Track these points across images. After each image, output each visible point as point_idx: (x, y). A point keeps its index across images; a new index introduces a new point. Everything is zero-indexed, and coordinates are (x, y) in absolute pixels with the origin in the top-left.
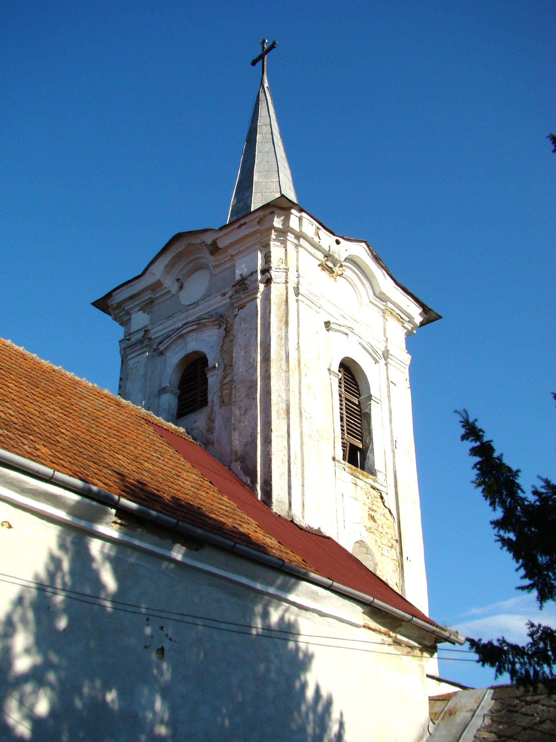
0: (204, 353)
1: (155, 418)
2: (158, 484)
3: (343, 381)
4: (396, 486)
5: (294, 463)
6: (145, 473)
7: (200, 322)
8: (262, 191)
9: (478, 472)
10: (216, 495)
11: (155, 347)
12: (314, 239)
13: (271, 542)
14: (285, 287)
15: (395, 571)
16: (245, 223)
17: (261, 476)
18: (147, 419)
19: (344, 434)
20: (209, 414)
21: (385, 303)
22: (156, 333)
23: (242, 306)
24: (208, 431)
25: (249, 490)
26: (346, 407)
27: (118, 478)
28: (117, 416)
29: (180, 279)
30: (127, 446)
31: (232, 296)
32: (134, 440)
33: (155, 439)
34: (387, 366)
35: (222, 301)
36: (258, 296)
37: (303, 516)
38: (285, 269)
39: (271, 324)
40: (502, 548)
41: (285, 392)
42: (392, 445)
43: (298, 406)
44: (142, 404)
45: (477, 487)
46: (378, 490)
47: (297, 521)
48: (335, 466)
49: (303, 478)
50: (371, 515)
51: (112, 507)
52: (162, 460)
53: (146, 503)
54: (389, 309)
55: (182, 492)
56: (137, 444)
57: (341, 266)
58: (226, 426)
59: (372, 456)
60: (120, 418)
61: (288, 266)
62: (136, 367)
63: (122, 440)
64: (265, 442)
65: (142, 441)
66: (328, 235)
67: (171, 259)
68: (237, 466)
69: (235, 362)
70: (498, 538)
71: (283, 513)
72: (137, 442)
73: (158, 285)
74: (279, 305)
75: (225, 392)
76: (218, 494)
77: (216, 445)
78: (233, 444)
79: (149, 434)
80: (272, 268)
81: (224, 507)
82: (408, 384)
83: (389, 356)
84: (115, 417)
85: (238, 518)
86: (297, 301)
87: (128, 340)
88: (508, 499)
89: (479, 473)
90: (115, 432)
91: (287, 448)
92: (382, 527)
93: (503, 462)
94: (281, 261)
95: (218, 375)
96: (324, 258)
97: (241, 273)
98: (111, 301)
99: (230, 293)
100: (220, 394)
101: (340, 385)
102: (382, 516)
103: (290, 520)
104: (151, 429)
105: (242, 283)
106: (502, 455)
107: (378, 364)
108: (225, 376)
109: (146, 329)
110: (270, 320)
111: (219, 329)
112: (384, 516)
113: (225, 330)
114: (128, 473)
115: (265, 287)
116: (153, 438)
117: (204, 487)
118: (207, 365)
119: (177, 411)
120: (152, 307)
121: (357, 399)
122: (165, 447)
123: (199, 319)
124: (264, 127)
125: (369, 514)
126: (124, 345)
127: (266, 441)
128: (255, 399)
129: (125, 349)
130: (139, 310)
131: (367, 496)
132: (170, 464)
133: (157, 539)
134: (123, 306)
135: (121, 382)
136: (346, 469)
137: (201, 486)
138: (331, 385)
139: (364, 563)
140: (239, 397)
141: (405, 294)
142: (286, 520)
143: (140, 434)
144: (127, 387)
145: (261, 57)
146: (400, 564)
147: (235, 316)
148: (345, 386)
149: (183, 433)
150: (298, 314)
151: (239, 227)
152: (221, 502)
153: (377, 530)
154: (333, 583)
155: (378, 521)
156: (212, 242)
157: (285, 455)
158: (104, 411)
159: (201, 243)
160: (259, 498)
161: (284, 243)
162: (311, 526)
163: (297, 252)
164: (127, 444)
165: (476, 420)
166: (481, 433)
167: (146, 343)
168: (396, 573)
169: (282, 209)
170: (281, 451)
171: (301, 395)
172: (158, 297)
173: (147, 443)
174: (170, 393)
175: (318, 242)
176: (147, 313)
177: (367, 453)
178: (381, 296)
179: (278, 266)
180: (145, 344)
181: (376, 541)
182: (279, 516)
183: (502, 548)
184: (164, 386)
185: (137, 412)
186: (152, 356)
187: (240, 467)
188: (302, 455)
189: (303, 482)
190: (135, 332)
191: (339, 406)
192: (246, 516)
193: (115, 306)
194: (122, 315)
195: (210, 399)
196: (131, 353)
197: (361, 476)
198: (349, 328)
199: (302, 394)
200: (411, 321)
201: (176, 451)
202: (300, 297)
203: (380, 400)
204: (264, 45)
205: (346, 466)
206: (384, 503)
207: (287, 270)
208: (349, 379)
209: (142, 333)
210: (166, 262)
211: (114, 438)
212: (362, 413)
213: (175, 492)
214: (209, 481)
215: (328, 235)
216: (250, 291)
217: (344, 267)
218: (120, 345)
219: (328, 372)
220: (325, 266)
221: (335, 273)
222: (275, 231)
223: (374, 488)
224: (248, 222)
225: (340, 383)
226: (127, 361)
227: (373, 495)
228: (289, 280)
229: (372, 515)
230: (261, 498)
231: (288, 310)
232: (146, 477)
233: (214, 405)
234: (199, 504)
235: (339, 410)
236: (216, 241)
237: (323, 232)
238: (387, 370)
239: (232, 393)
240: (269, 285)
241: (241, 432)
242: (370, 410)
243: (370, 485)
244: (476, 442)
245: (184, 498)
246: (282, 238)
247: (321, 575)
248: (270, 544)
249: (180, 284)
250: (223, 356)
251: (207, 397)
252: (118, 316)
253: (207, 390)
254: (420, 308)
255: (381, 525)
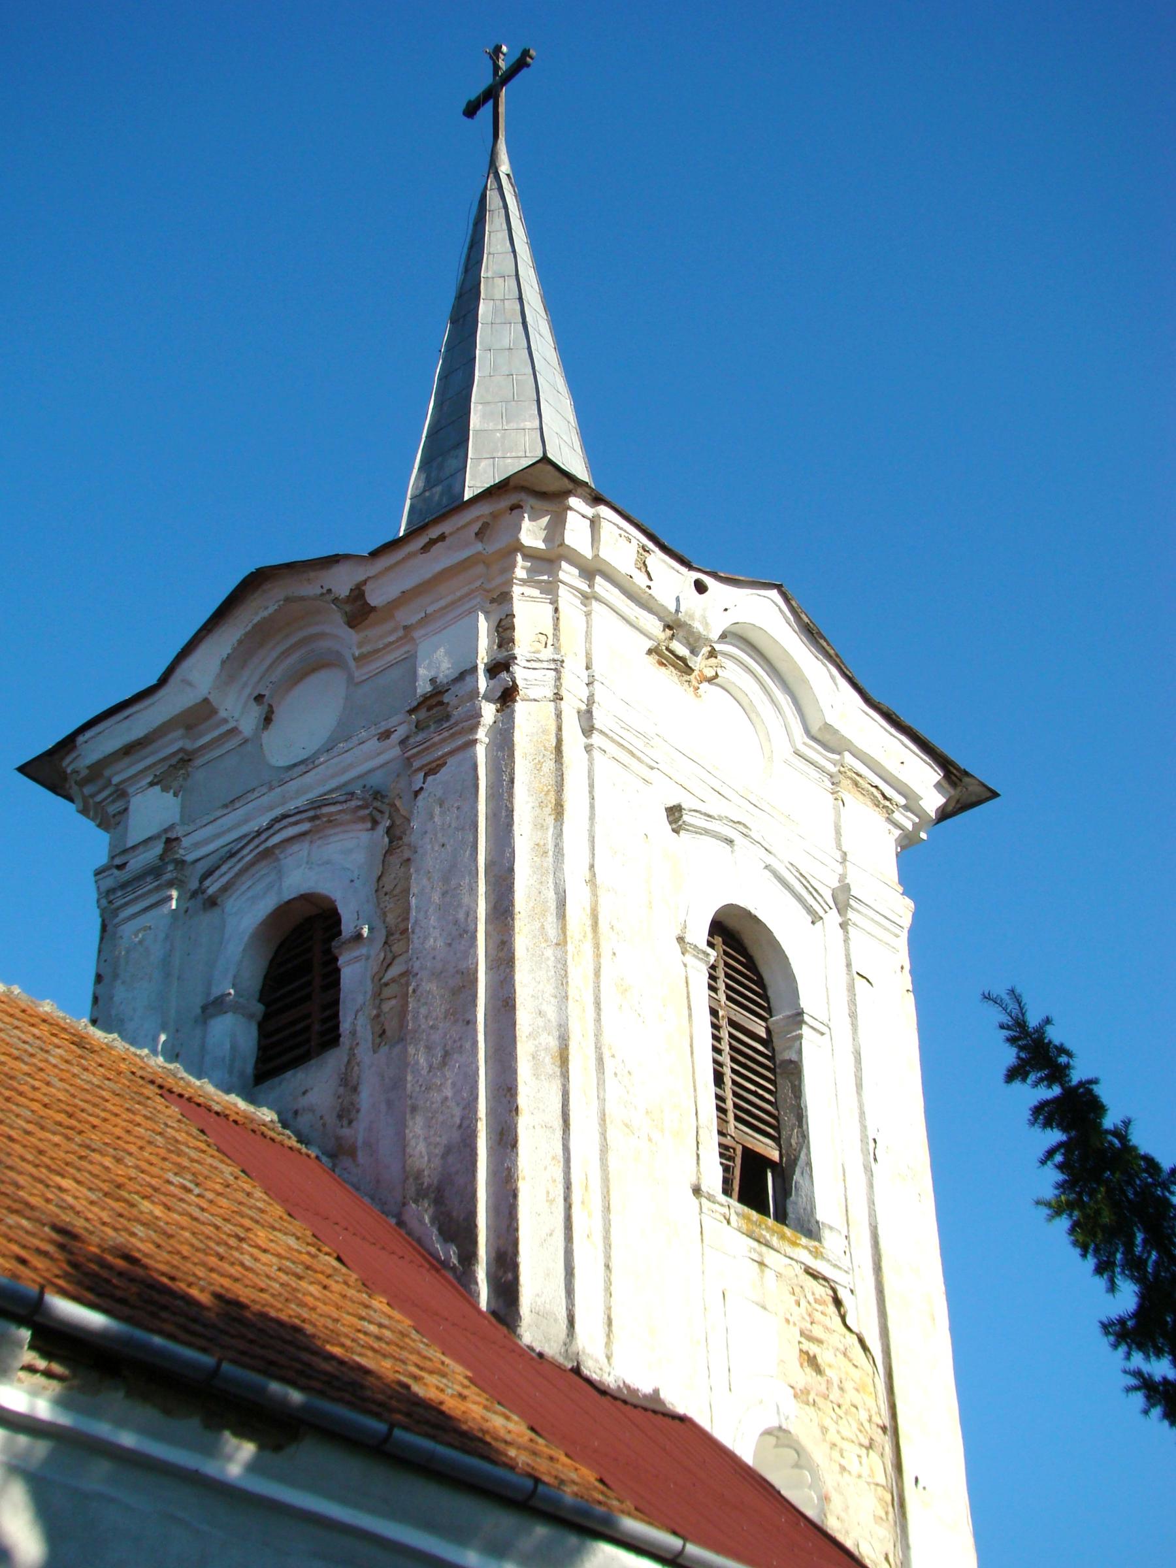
0: (331, 899)
1: (188, 1084)
2: (176, 1260)
3: (720, 974)
4: (878, 1269)
5: (583, 1203)
6: (139, 1230)
7: (318, 812)
8: (495, 455)
9: (1059, 1177)
10: (351, 1292)
11: (194, 885)
12: (635, 580)
13: (506, 1428)
14: (553, 711)
15: (881, 1518)
16: (442, 538)
17: (487, 1241)
18: (165, 1084)
19: (727, 1122)
20: (343, 1070)
21: (837, 757)
22: (197, 845)
23: (434, 765)
24: (340, 1117)
25: (455, 1282)
26: (730, 1044)
27: (52, 1241)
28: (74, 1075)
29: (264, 695)
30: (92, 1154)
31: (408, 737)
32: (119, 1138)
33: (180, 1138)
34: (846, 932)
35: (379, 754)
36: (477, 737)
37: (609, 1354)
38: (554, 660)
39: (515, 813)
40: (1146, 1412)
41: (553, 1000)
42: (865, 1152)
43: (592, 1040)
44: (157, 1045)
45: (1053, 1217)
46: (825, 1279)
47: (591, 1369)
48: (701, 1211)
49: (608, 1245)
50: (807, 1353)
51: (22, 1321)
52: (199, 1196)
53: (127, 1311)
54: (849, 774)
55: (248, 1282)
56: (125, 1150)
57: (713, 654)
58: (389, 1103)
59: (807, 1183)
60: (83, 1080)
61: (562, 653)
62: (140, 942)
63: (78, 1139)
64: (499, 1144)
65: (140, 1143)
66: (673, 568)
67: (240, 642)
68: (423, 1216)
69: (416, 921)
70: (1133, 1381)
71: (550, 1347)
72: (127, 1146)
73: (203, 712)
74: (536, 761)
75: (386, 1007)
76: (359, 1291)
77: (361, 1156)
78: (408, 1150)
79: (166, 1125)
80: (516, 658)
81: (372, 1328)
82: (906, 981)
83: (852, 902)
84: (65, 1075)
85: (414, 1358)
86: (588, 749)
87: (120, 867)
88: (1149, 1253)
89: (1065, 1181)
90: (61, 1117)
91: (562, 1160)
92: (841, 1389)
93: (1131, 1143)
94: (543, 638)
95: (368, 958)
96: (664, 630)
97: (432, 674)
98: (75, 759)
99: (401, 732)
100: (375, 1012)
101: (712, 983)
102: (840, 1356)
103: (570, 1366)
104: (174, 1110)
105: (433, 701)
106: (1127, 1123)
107: (819, 924)
108: (388, 961)
109: (169, 835)
110: (512, 803)
111: (371, 832)
112: (845, 1354)
113: (387, 833)
114: (86, 1229)
115: (498, 711)
116: (177, 1135)
117: (316, 1271)
118: (340, 933)
119: (257, 1062)
120: (187, 776)
121: (763, 1024)
122: (210, 1160)
123: (317, 804)
124: (500, 281)
125: (801, 1351)
126: (109, 883)
127: (501, 1140)
128: (471, 1023)
129: (111, 891)
130: (152, 784)
131: (794, 1298)
132: (221, 1207)
133: (148, 1413)
134: (107, 773)
135: (98, 986)
136: (734, 1218)
137: (308, 1268)
138: (687, 983)
139: (783, 1492)
140: (426, 1017)
141: (893, 730)
142: (559, 1367)
143: (139, 1125)
144: (115, 999)
145: (491, 94)
146: (896, 1498)
147: (417, 793)
148: (728, 987)
149: (271, 1125)
150: (591, 786)
151: (426, 549)
152: (364, 1314)
153: (826, 1397)
154: (684, 1546)
155: (828, 1371)
156: (351, 590)
157: (554, 1181)
158: (35, 1061)
159: (322, 594)
160: (483, 1304)
161: (550, 590)
162: (632, 1386)
163: (588, 614)
164: (94, 1150)
165: (1048, 1021)
166: (1063, 1059)
167: (169, 874)
168: (885, 1524)
169: (543, 495)
170: (545, 1168)
171: (600, 1009)
172: (203, 747)
173: (157, 1149)
174: (234, 1013)
175: (644, 587)
176: (172, 791)
177: (794, 1174)
178: (827, 737)
179: (534, 653)
180: (168, 877)
181: (824, 1430)
182: (541, 1355)
183: (1146, 1412)
184: (219, 994)
185: (135, 1065)
186: (186, 911)
187: (430, 1218)
188: (606, 1180)
189: (608, 1257)
190: (139, 844)
191: (710, 1041)
192: (439, 1355)
193: (84, 773)
194: (104, 800)
195: (345, 1026)
196: (126, 904)
197: (775, 1241)
198: (737, 825)
199: (602, 1006)
200: (912, 804)
201: (243, 1171)
202: (596, 739)
203: (828, 1026)
204: (498, 58)
205: (732, 1211)
206: (843, 1318)
207: (559, 663)
208: (740, 967)
209: (158, 848)
210: (226, 650)
211: (54, 1133)
212: (778, 1062)
213: (227, 1282)
214: (335, 1255)
215: (673, 568)
216: (456, 724)
217: (719, 657)
218: (96, 882)
219: (677, 948)
220: (667, 653)
221: (696, 673)
222: (526, 557)
223: (815, 1275)
224: (451, 534)
225: (712, 977)
226: (117, 926)
227: (813, 1294)
228: (564, 693)
229: (811, 1354)
230: (488, 1303)
231: (562, 774)
232: (141, 1240)
233: (358, 1044)
234: (296, 1317)
235: (710, 1054)
236: (363, 588)
237: (658, 560)
238: (846, 940)
239: (408, 1007)
240: (508, 707)
241: (432, 1118)
242: (800, 1052)
243: (803, 1267)
244: (1049, 1087)
245: (253, 1301)
246: (545, 577)
247: (650, 1523)
248: (502, 1433)
249: (266, 707)
250: (382, 905)
251: (339, 1023)
252: (91, 801)
253: (336, 1002)
254: (937, 769)
255: (836, 1382)
